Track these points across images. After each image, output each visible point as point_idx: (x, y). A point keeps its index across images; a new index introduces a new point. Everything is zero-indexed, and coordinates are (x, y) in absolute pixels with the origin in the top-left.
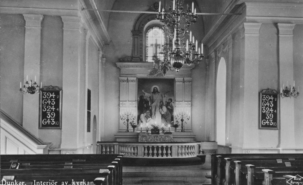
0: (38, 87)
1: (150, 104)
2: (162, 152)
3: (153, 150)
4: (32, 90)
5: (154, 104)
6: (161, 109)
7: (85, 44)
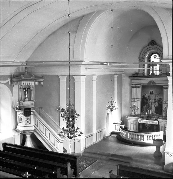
0: (63, 130)
3: (150, 137)
5: (151, 100)
6: (155, 104)
7: (88, 23)
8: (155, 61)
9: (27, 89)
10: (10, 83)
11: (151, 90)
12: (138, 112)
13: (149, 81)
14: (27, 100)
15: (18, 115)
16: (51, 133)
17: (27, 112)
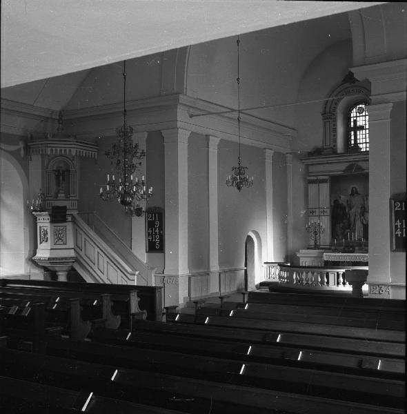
1: (347, 210)
6: (362, 218)
8: (360, 122)
9: (61, 172)
10: (22, 152)
11: (352, 186)
12: (325, 238)
13: (348, 164)
14: (61, 196)
15: (39, 225)
16: (110, 262)
17: (58, 216)
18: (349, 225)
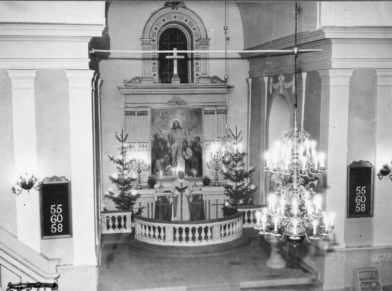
1: (168, 145)
2: (114, 224)
3: (119, 220)
4: (27, 186)
6: (184, 153)
18: (171, 160)
